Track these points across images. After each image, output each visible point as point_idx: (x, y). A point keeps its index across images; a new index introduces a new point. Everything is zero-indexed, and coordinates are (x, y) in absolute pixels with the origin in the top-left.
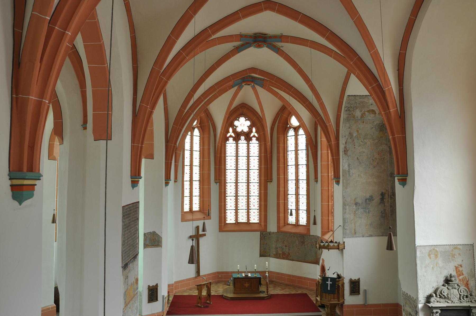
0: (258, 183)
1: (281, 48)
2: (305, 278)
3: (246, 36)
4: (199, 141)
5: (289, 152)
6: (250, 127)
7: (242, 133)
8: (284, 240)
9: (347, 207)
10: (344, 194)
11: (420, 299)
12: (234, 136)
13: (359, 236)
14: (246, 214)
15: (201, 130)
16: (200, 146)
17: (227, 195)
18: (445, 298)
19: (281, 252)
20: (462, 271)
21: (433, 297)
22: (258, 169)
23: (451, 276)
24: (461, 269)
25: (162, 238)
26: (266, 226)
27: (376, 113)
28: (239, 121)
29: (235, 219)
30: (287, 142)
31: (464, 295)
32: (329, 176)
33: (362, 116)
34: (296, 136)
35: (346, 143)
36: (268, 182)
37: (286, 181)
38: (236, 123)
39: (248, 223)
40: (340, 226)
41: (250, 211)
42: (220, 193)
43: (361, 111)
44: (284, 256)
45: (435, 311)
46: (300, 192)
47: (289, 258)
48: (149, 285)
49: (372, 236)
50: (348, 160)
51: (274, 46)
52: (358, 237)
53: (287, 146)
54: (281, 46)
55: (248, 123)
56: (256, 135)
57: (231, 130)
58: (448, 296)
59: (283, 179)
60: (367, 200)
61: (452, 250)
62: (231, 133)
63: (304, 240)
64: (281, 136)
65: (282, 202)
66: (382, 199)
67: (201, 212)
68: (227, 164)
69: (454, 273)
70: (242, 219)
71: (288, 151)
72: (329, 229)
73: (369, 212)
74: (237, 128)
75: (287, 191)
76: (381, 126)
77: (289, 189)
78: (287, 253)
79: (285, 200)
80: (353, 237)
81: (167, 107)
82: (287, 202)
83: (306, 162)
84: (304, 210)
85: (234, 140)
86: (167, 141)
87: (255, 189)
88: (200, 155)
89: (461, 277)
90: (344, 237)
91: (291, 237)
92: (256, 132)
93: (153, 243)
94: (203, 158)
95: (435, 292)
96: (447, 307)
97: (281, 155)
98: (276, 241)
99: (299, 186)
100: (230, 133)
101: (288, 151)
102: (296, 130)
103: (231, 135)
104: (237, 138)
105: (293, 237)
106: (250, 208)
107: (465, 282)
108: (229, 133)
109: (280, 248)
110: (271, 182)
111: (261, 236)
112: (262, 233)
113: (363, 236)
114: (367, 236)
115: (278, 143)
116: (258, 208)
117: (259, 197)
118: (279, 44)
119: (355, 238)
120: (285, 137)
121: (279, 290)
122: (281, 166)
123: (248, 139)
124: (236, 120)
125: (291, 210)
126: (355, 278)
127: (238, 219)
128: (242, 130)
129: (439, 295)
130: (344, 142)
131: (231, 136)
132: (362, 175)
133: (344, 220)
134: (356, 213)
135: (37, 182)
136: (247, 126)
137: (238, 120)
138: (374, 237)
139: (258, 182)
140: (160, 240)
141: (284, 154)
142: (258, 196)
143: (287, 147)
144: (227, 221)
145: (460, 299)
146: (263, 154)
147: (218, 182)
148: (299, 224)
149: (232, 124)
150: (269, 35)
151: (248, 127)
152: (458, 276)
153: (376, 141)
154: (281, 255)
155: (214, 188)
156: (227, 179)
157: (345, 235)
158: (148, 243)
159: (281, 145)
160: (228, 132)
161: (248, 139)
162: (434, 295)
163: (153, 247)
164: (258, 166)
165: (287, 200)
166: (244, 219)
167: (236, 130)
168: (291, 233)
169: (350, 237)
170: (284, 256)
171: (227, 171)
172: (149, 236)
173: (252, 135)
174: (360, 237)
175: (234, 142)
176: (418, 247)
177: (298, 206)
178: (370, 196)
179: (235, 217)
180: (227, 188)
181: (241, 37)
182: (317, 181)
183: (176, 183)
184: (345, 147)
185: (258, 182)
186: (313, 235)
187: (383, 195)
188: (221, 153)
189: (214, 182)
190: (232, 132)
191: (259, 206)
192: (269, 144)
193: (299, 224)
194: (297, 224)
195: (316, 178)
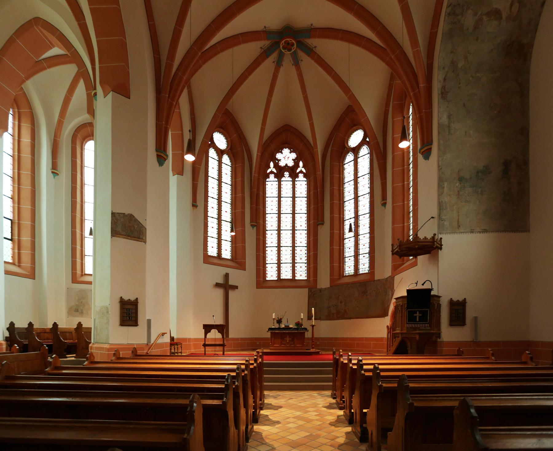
0: (306, 230)
2: (367, 339)
4: (231, 173)
8: (339, 295)
9: (446, 185)
10: (440, 163)
12: (275, 171)
13: (465, 231)
14: (291, 268)
16: (232, 179)
22: (306, 212)
25: (146, 229)
26: (315, 281)
27: (501, 18)
28: (282, 153)
29: (278, 276)
32: (405, 185)
33: (476, 27)
35: (445, 80)
36: (318, 225)
38: (279, 156)
39: (293, 279)
40: (432, 218)
41: (296, 265)
42: (258, 240)
48: (121, 297)
49: (487, 232)
50: (447, 107)
52: (463, 232)
55: (294, 155)
56: (304, 171)
57: (272, 164)
60: (480, 174)
65: (336, 247)
68: (266, 206)
70: (286, 274)
77: (346, 232)
78: (342, 311)
80: (455, 233)
81: (154, 25)
83: (369, 189)
84: (366, 253)
87: (302, 238)
88: (232, 190)
90: (440, 233)
93: (129, 232)
94: (235, 194)
97: (336, 188)
100: (270, 168)
103: (272, 171)
104: (279, 176)
106: (296, 262)
108: (270, 169)
109: (333, 307)
111: (310, 294)
112: (311, 290)
113: (471, 232)
114: (479, 232)
115: (332, 172)
116: (306, 262)
117: (307, 248)
119: (458, 234)
123: (294, 176)
126: (457, 297)
127: (281, 275)
128: (286, 165)
130: (441, 77)
131: (272, 172)
132: (471, 132)
133: (441, 206)
134: (460, 194)
136: (293, 160)
138: (490, 232)
139: (306, 229)
140: (142, 232)
141: (339, 187)
142: (306, 247)
144: (267, 277)
155: (250, 233)
156: (267, 225)
157: (441, 228)
158: (119, 229)
159: (336, 175)
161: (294, 176)
163: (129, 239)
164: (306, 209)
165: (343, 246)
166: (289, 275)
169: (450, 233)
171: (267, 215)
172: (122, 220)
174: (467, 233)
175: (276, 180)
178: (484, 167)
179: (277, 272)
180: (267, 237)
182: (384, 204)
184: (444, 87)
185: (306, 229)
186: (379, 280)
187: (506, 165)
188: (258, 190)
190: (273, 167)
191: (307, 259)
192: (319, 173)
195: (384, 197)
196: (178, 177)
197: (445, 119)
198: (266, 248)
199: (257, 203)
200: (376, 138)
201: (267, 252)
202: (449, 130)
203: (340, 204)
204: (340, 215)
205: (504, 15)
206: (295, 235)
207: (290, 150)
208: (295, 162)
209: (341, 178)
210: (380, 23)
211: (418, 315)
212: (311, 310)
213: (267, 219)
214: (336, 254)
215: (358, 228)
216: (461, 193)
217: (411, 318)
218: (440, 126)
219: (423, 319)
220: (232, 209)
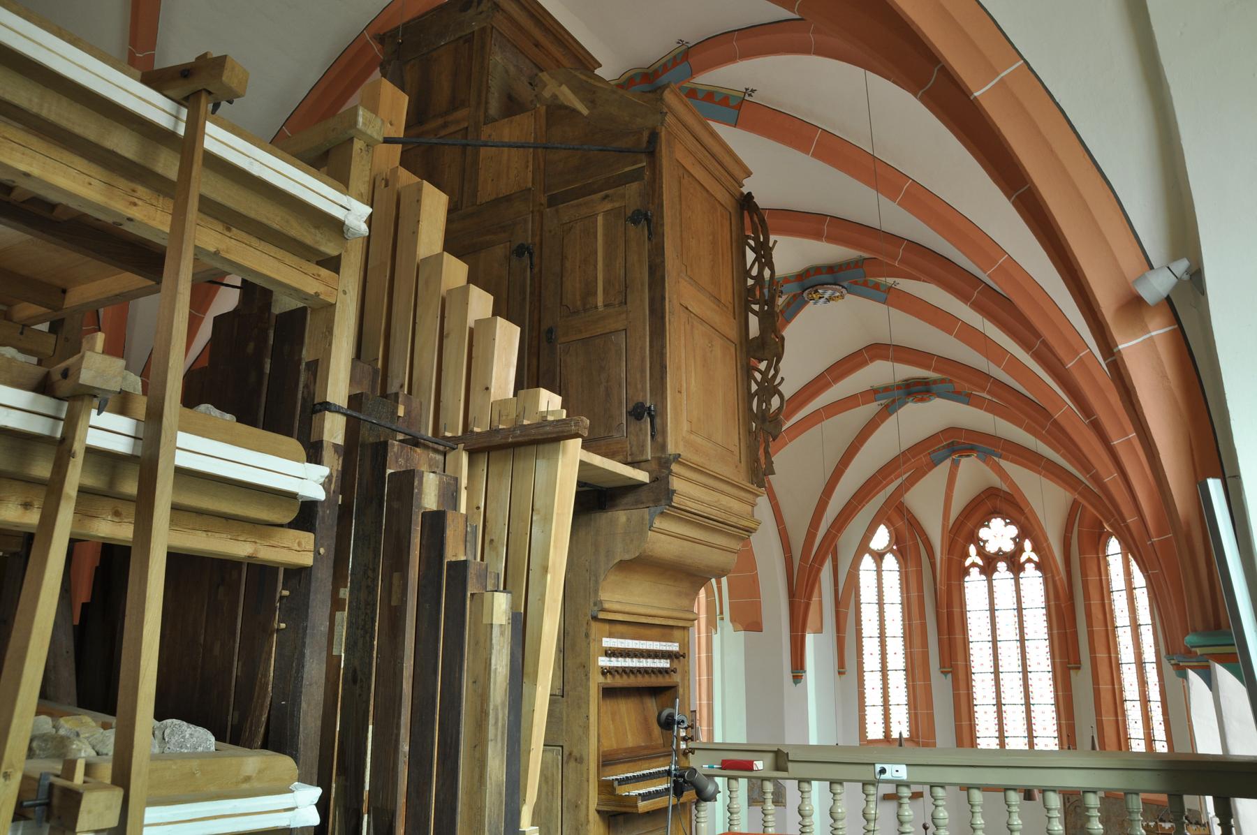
3: (887, 389)
6: (1018, 540)
7: (1000, 556)
12: (980, 562)
15: (901, 558)
16: (902, 592)
17: (975, 703)
25: (785, 788)
34: (879, 572)
36: (1070, 669)
37: (1115, 666)
38: (983, 533)
42: (956, 698)
53: (1108, 580)
55: (1013, 531)
56: (1035, 558)
57: (972, 549)
59: (1106, 661)
62: (973, 557)
64: (1091, 556)
67: (913, 741)
71: (1112, 592)
74: (987, 544)
75: (1121, 691)
79: (1116, 715)
82: (1124, 721)
85: (981, 573)
86: (792, 594)
92: (1034, 550)
97: (1095, 602)
98: (1105, 820)
101: (1112, 592)
104: (988, 568)
108: (970, 558)
110: (1079, 668)
111: (1067, 806)
112: (1068, 799)
115: (1084, 574)
120: (1101, 558)
122: (1098, 628)
123: (1016, 567)
124: (984, 526)
131: (974, 565)
135: (803, 674)
136: (1011, 539)
137: (988, 526)
141: (908, 598)
143: (1109, 583)
146: (1052, 603)
147: (949, 672)
149: (973, 536)
151: (1014, 539)
159: (1093, 578)
160: (967, 555)
161: (1016, 567)
165: (1124, 715)
167: (985, 550)
171: (971, 645)
173: (1023, 559)
175: (983, 577)
177: (1150, 730)
181: (875, 394)
183: (843, 676)
196: (815, 638)
198: (975, 707)
199: (951, 631)
201: (976, 715)
206: (1028, 688)
207: (1002, 552)
208: (1016, 544)
213: (971, 652)
215: (1144, 687)
220: (907, 679)
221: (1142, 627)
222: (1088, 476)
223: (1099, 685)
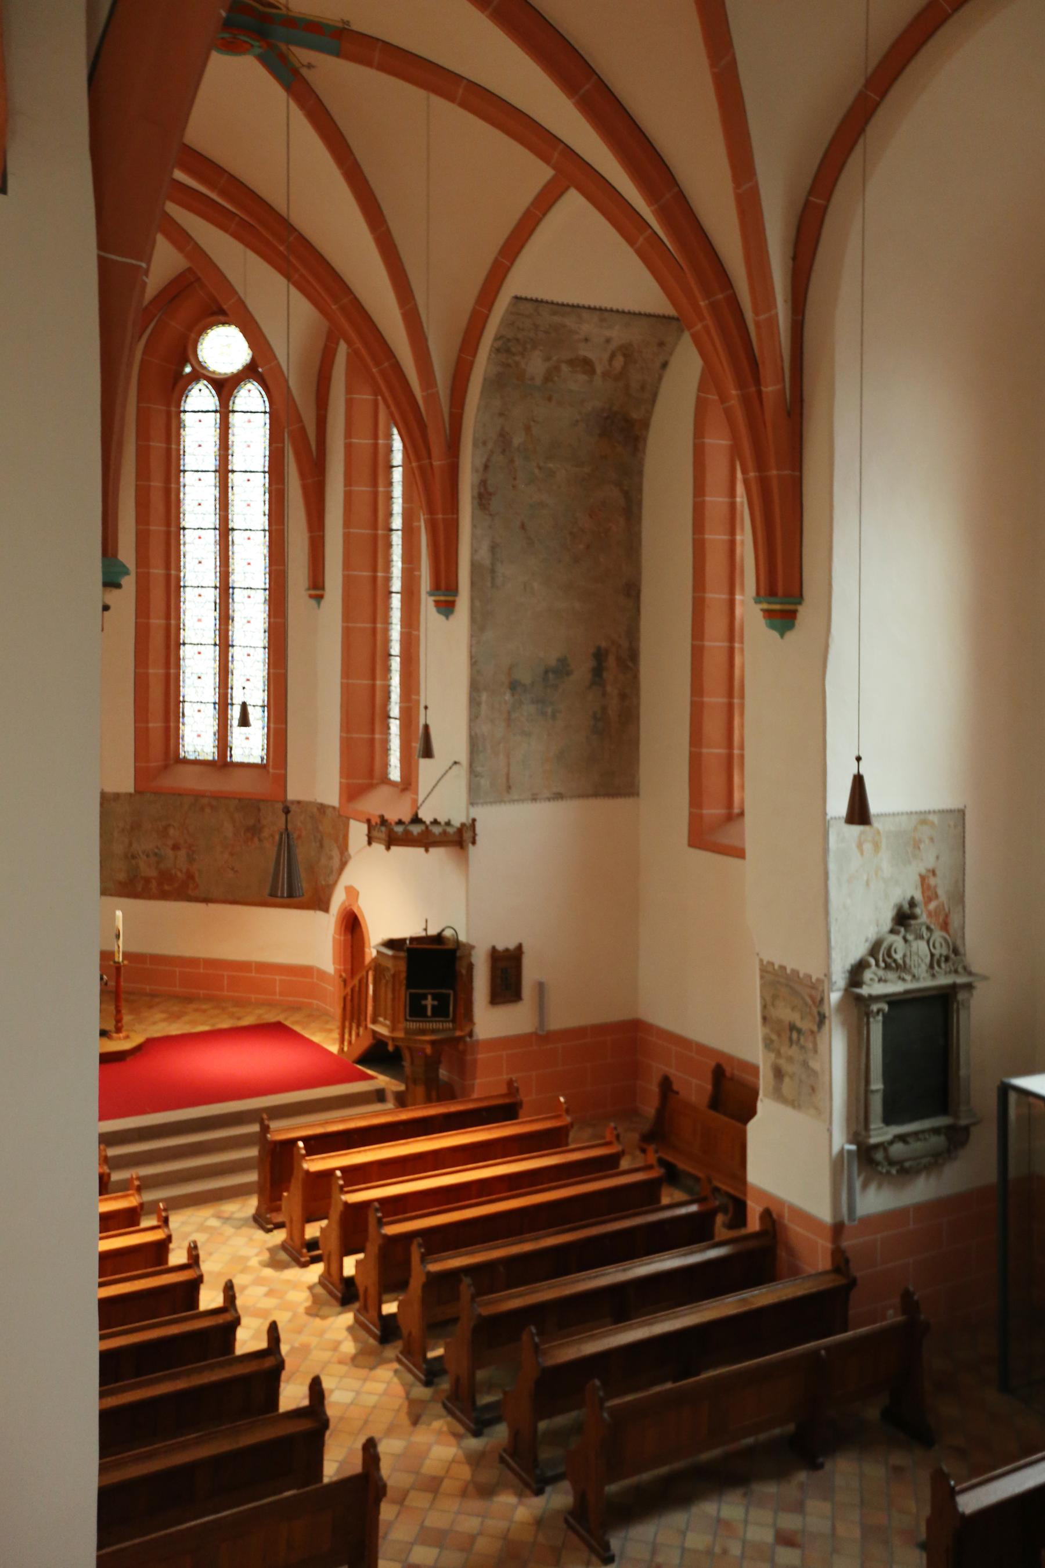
1: (304, 72)
2: (263, 967)
5: (186, 473)
8: (169, 825)
9: (484, 697)
11: (834, 978)
18: (898, 967)
19: (152, 873)
20: (935, 887)
21: (869, 966)
23: (912, 903)
24: (932, 881)
30: (179, 435)
31: (941, 955)
33: (548, 378)
34: (225, 412)
35: (486, 467)
40: (455, 763)
43: (548, 359)
44: (166, 887)
45: (875, 1007)
46: (234, 637)
47: (190, 892)
50: (490, 527)
51: (283, 58)
52: (518, 801)
53: (179, 450)
54: (305, 63)
58: (904, 962)
61: (915, 829)
63: (259, 821)
65: (155, 671)
66: (598, 672)
69: (918, 896)
71: (215, 471)
72: (371, 773)
73: (554, 717)
76: (607, 418)
78: (179, 874)
89: (932, 906)
91: (202, 809)
95: (874, 951)
96: (907, 992)
97: (157, 484)
99: (233, 611)
102: (225, 392)
105: (208, 810)
107: (941, 920)
109: (148, 856)
115: (143, 434)
118: (302, 55)
121: (164, 1020)
125: (244, 706)
129: (884, 961)
132: (536, 585)
141: (168, 480)
145: (931, 966)
148: (229, 759)
150: (284, 11)
152: (927, 903)
153: (587, 470)
154: (154, 884)
157: (475, 795)
159: (157, 445)
162: (872, 961)
168: (198, 795)
170: (166, 887)
176: (831, 822)
177: (227, 688)
184: (483, 483)
187: (600, 656)
189: (307, 598)
193: (232, 762)
194: (223, 763)
195: (317, 585)
197: (484, 553)
200: (300, 419)
202: (493, 579)
203: (168, 534)
204: (168, 567)
205: (599, 370)
209: (174, 453)
210: (347, 290)
211: (429, 1002)
212: (113, 918)
214: (156, 692)
215: (227, 624)
216: (514, 715)
217: (416, 1010)
218: (475, 566)
219: (441, 1011)
221: (235, 532)
222: (144, 265)
223: (148, 617)
